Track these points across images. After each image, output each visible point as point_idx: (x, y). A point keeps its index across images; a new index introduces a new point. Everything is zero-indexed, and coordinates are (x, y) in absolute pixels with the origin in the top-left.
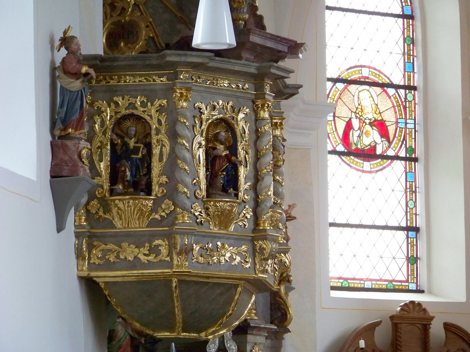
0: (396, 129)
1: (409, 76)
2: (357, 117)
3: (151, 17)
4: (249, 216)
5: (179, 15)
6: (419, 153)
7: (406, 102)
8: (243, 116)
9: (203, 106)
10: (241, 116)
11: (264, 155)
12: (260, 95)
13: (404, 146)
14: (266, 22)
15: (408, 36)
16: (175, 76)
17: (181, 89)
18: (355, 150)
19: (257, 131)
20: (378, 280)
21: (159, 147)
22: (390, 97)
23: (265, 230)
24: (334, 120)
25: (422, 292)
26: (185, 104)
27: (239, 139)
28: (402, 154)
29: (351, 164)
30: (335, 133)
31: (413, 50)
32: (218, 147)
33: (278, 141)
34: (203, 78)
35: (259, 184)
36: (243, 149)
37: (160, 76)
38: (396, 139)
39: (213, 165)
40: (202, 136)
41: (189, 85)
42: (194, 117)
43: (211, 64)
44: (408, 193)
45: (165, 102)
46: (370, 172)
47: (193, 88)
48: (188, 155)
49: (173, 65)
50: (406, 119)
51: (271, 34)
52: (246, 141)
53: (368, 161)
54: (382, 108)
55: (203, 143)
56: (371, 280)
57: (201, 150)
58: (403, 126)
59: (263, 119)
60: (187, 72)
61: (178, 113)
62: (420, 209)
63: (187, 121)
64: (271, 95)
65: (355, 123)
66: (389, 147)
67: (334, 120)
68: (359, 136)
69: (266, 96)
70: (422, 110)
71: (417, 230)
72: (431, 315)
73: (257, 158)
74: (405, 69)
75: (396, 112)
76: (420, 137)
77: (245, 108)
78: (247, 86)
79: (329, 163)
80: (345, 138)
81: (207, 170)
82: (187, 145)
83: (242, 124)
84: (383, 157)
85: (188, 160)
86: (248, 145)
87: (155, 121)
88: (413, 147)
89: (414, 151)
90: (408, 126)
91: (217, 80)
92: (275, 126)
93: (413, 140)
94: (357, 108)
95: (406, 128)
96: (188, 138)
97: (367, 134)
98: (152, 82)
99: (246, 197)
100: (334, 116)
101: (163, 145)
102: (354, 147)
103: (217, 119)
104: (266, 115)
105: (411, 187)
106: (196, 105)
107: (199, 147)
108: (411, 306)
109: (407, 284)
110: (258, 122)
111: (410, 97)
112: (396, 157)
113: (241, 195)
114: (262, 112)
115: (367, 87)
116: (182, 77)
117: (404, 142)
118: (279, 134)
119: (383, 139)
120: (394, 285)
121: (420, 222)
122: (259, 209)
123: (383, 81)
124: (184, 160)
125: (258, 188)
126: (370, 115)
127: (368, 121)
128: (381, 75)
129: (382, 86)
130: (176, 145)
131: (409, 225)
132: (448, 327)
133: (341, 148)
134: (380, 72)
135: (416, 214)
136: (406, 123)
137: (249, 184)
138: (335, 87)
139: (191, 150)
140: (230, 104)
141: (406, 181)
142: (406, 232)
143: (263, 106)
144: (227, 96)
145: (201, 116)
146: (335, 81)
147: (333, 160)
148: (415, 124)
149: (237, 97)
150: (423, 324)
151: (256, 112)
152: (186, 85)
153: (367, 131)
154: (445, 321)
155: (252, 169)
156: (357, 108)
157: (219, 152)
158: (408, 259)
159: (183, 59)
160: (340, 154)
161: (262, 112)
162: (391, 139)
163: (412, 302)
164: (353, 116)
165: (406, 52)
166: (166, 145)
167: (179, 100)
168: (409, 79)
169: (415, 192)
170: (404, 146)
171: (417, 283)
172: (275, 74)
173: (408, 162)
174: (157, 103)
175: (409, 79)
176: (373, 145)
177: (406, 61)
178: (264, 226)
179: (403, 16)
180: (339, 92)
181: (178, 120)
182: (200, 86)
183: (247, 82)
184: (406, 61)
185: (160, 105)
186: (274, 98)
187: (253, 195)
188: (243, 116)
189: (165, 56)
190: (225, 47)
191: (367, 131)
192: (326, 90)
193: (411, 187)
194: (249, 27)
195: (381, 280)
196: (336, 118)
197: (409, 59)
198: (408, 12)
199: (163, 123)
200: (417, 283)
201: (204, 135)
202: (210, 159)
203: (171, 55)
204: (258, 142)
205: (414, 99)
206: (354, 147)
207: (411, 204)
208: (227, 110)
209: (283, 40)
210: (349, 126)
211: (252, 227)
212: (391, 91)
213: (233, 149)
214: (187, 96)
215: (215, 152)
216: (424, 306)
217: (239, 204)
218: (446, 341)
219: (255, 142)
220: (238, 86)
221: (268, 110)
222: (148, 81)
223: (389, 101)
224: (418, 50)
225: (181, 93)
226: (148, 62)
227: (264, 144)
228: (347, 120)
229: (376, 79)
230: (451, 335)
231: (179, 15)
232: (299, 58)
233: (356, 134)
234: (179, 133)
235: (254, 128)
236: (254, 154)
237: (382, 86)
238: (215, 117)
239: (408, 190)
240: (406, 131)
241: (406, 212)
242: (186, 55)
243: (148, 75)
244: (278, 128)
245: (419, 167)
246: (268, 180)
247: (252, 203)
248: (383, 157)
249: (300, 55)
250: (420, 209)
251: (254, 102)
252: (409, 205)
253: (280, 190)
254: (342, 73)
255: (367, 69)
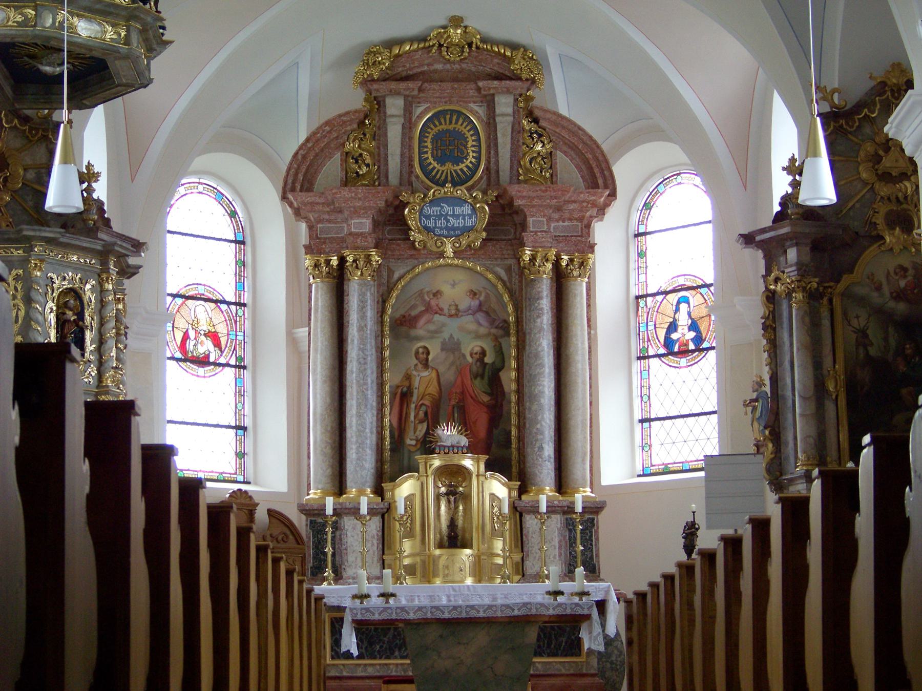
0: (228, 340)
1: (240, 294)
2: (193, 328)
3: (11, 218)
4: (93, 374)
5: (36, 216)
6: (248, 361)
7: (236, 316)
8: (90, 287)
9: (54, 276)
10: (88, 287)
11: (108, 321)
12: (106, 270)
13: (234, 355)
14: (113, 224)
15: (239, 259)
16: (31, 249)
17: (36, 260)
18: (191, 357)
19: (102, 301)
20: (210, 472)
21: (16, 311)
22: (222, 312)
23: (108, 386)
24: (173, 330)
25: (249, 483)
26: (39, 274)
27: (86, 307)
28: (233, 362)
29: (187, 370)
30: (174, 341)
31: (244, 272)
32: (67, 313)
33: (120, 314)
34: (55, 252)
35: (102, 347)
36: (89, 315)
37: (17, 249)
38: (227, 349)
39: (63, 329)
40: (53, 302)
41: (43, 257)
42: (47, 285)
43: (62, 240)
44: (237, 396)
45: (21, 271)
46: (204, 377)
47: (46, 260)
48: (40, 318)
49: (28, 239)
50: (236, 331)
51: (116, 233)
52: (92, 309)
53: (203, 367)
54: (215, 321)
55: (54, 308)
56: (203, 472)
57: (52, 314)
58: (234, 337)
59: (107, 290)
60: (41, 246)
61: (32, 282)
62: (248, 410)
63: (41, 288)
64: (114, 270)
65: (192, 334)
66: (221, 355)
67: (173, 330)
68: (195, 345)
69: (111, 271)
70: (251, 348)
71: (244, 429)
72: (256, 502)
73: (102, 324)
74: (236, 288)
75: (227, 325)
76: (248, 348)
77: (91, 280)
78: (94, 261)
79: (168, 368)
80: (183, 347)
81: (57, 333)
82: (40, 309)
83: (88, 294)
84: (216, 364)
85: (41, 322)
86: (94, 312)
87: (12, 288)
88: (243, 356)
89: (243, 359)
90: (239, 338)
91: (67, 255)
92: (118, 301)
93: (243, 350)
94: (193, 321)
95: (236, 339)
96: (41, 303)
97: (202, 343)
98: (10, 254)
99: (92, 357)
100: (173, 327)
101: (19, 309)
102: (190, 355)
103: (67, 289)
104: (110, 287)
105: (240, 391)
106: (49, 275)
107: (51, 312)
108: (238, 493)
109: (235, 476)
110: (102, 293)
111: (240, 313)
112: (228, 365)
113: (87, 355)
114: (106, 284)
115: (202, 302)
116: (36, 250)
117: (235, 352)
118: (121, 307)
119: (216, 349)
120: (224, 477)
121: (248, 422)
122: (102, 368)
123: (217, 298)
124: (38, 322)
125: (102, 350)
126: (204, 327)
127: (202, 333)
128: (215, 292)
129: (216, 302)
130: (30, 308)
131: (238, 424)
132: (270, 512)
133: (178, 355)
134: (214, 290)
135: (244, 415)
136: (236, 335)
137: (94, 346)
138: (174, 302)
139: (43, 314)
140: (79, 276)
141: (236, 386)
142: (235, 430)
143: (107, 279)
144: (76, 269)
145: (52, 284)
146: (175, 296)
147: (171, 364)
148: (244, 336)
149: (85, 271)
150: (249, 510)
151: (101, 284)
152: (40, 257)
153: (202, 341)
154: (269, 507)
155: (97, 333)
156: (193, 321)
157: (68, 317)
158: (237, 454)
159: (38, 234)
160: (178, 360)
161: (106, 284)
162: (223, 349)
163: (240, 490)
164: (190, 327)
165: (238, 273)
166: (21, 309)
167: (34, 269)
168: (240, 297)
169: (244, 395)
170: (234, 355)
171: (244, 476)
172: (118, 251)
173: (237, 245)
174: (14, 272)
175: (240, 297)
176: (207, 353)
177: (237, 377)
178: (107, 383)
179: (236, 242)
180: (178, 306)
181: (32, 287)
182: (53, 259)
183: (93, 258)
184: (237, 377)
185: (17, 274)
186: (118, 273)
187: (98, 356)
188: (90, 287)
189: (21, 230)
190: (74, 211)
191: (202, 341)
192: (166, 303)
193: (240, 391)
194: (97, 225)
195: (212, 472)
196: (175, 329)
197: (240, 279)
198: (240, 238)
199: (19, 289)
200: (244, 476)
201: (55, 301)
202: (60, 323)
203: (27, 230)
204: (103, 311)
205: (244, 315)
206: (190, 355)
207: (240, 406)
208: (76, 281)
209: (128, 239)
210: (186, 337)
211: (96, 383)
212: (224, 307)
213: (81, 315)
214: (40, 267)
215: (65, 317)
216: (250, 494)
217: (85, 362)
218: (269, 526)
219: (100, 311)
220: (86, 261)
221: (112, 283)
222: (6, 253)
223: (221, 315)
224: (248, 272)
225: (36, 264)
226: (6, 236)
227: (108, 311)
228: (184, 330)
229: (211, 296)
230: (274, 520)
231: (36, 216)
232: (141, 256)
233: (193, 343)
234: (33, 298)
235: (99, 298)
236: (99, 321)
237: (216, 302)
238: (65, 287)
239: (237, 394)
240: (236, 342)
241: (236, 413)
242: (40, 230)
243: (6, 248)
244: (120, 303)
245: (247, 374)
246: (111, 343)
247: (97, 363)
248: (216, 364)
249: (143, 254)
250: (248, 410)
251: (99, 276)
252: (238, 407)
253: (122, 356)
254: (181, 289)
255: (203, 287)
